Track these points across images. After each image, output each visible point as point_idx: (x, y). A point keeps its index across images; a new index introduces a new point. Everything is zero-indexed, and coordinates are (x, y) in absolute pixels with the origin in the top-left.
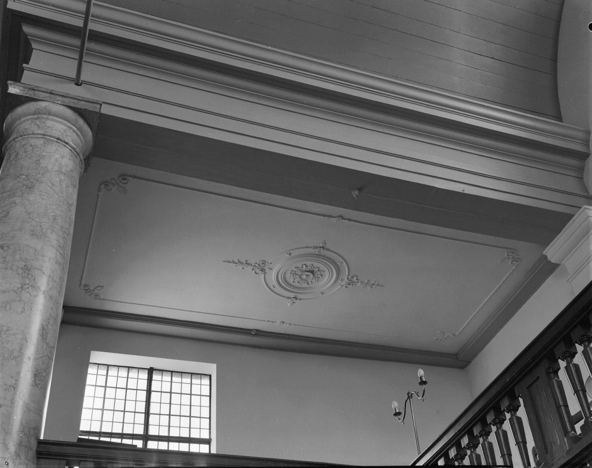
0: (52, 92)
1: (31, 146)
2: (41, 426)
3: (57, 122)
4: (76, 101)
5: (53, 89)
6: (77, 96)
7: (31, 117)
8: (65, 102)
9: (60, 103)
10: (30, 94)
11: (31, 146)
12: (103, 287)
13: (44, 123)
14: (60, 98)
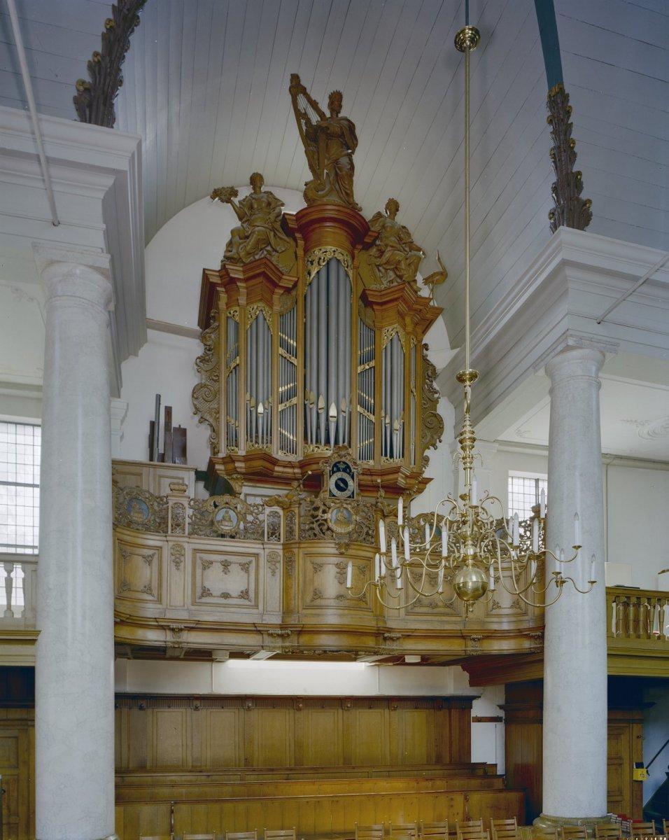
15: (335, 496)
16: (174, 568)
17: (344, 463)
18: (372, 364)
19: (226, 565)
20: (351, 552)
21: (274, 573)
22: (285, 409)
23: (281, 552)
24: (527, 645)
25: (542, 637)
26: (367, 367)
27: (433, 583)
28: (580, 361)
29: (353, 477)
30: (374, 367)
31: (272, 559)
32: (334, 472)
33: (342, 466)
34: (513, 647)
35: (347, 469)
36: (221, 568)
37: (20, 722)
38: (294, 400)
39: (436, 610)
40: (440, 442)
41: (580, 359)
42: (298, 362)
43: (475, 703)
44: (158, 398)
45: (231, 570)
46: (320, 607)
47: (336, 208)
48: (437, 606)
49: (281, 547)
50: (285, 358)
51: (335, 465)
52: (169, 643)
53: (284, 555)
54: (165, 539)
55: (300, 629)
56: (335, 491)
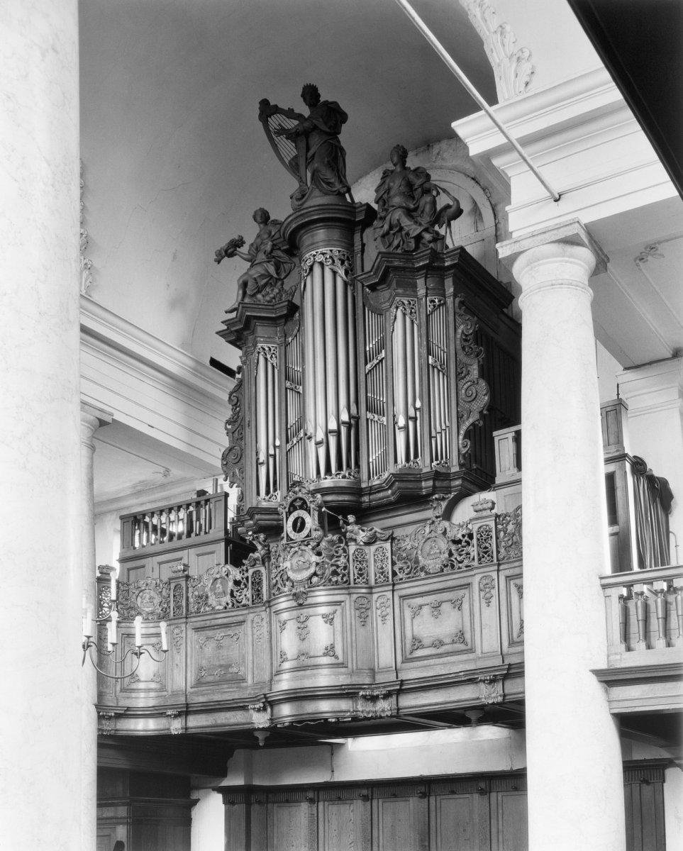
33: (298, 504)
34: (161, 727)
37: (326, 815)
46: (133, 690)
47: (344, 208)
48: (441, 643)
55: (505, 672)
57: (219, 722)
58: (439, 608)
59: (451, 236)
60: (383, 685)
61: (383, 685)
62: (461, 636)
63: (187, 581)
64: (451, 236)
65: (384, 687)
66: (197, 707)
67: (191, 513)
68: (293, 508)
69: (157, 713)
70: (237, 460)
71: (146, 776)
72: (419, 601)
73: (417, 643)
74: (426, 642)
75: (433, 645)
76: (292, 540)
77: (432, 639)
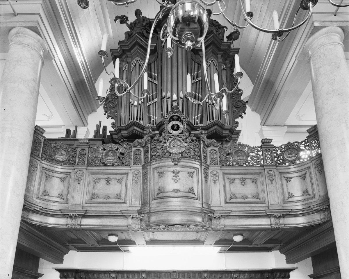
0: (332, 21)
1: (330, 49)
2: (141, 44)
3: (335, 35)
4: (341, 23)
5: (331, 19)
6: (342, 20)
7: (324, 36)
8: (337, 25)
9: (336, 25)
10: (323, 24)
11: (330, 49)
12: (305, 115)
13: (330, 37)
14: (335, 23)
15: (171, 134)
16: (76, 183)
17: (177, 116)
18: (200, 78)
19: (108, 181)
20: (181, 164)
21: (136, 183)
22: (151, 104)
23: (141, 171)
24: (317, 218)
25: (328, 209)
26: (197, 80)
27: (243, 183)
28: (326, 35)
29: (182, 123)
30: (201, 80)
31: (135, 176)
32: (170, 121)
34: (307, 221)
35: (179, 119)
36: (105, 182)
38: (156, 100)
39: (247, 200)
40: (245, 114)
41: (325, 34)
42: (158, 83)
43: (292, 274)
44: (100, 122)
45: (110, 183)
49: (141, 168)
50: (151, 82)
51: (171, 117)
52: (69, 226)
53: (143, 172)
54: (73, 168)
56: (171, 131)
57: (104, 224)
58: (245, 181)
59: (233, 45)
60: (219, 212)
61: (219, 212)
62: (257, 196)
63: (89, 148)
64: (233, 45)
65: (220, 213)
66: (92, 213)
67: (163, 37)
68: (172, 119)
69: (304, 213)
70: (111, 107)
71: (36, 244)
72: (233, 177)
73: (233, 196)
74: (237, 195)
75: (242, 197)
76: (170, 133)
77: (241, 195)
